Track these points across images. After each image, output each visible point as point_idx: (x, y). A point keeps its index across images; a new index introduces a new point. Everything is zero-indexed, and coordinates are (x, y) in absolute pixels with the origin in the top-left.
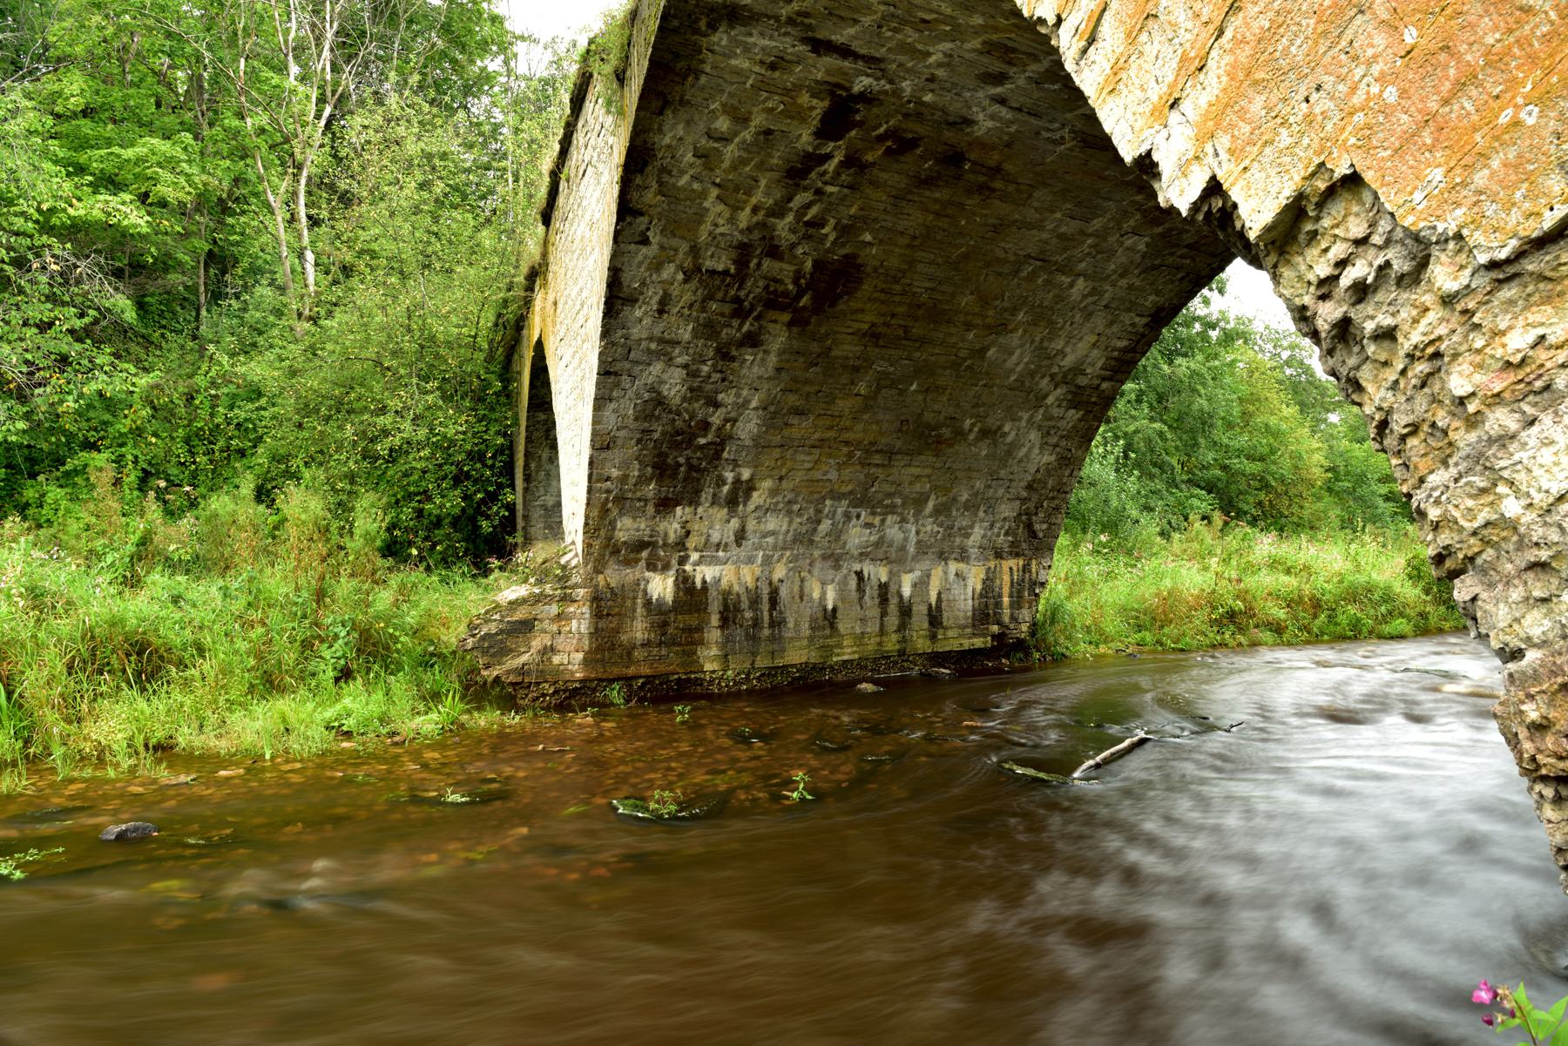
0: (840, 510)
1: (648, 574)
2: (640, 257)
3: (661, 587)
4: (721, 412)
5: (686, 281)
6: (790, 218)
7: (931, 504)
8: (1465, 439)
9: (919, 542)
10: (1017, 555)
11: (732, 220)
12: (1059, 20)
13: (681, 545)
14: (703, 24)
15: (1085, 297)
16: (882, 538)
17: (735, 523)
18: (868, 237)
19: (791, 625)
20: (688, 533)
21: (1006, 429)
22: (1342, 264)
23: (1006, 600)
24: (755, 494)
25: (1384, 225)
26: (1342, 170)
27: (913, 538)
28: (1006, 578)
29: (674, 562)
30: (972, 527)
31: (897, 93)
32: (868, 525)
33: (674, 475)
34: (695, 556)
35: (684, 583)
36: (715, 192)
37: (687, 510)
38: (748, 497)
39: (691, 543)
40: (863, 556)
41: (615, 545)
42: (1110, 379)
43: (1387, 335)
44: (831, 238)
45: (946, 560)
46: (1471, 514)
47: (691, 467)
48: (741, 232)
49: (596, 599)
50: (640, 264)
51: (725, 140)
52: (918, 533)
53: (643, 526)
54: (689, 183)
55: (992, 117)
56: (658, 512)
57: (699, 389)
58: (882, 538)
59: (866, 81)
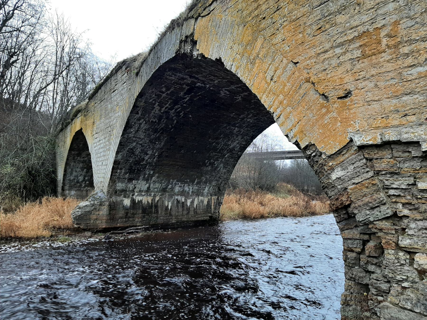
0: (174, 182)
1: (124, 199)
2: (136, 117)
3: (127, 202)
4: (148, 156)
5: (146, 123)
6: (174, 110)
7: (196, 182)
8: (326, 173)
9: (192, 191)
10: (216, 195)
11: (160, 110)
12: (273, 113)
13: (133, 191)
14: (167, 70)
15: (237, 132)
16: (183, 190)
17: (147, 185)
18: (190, 116)
19: (160, 213)
20: (135, 187)
21: (215, 163)
22: (312, 153)
23: (213, 207)
24: (153, 178)
25: (317, 150)
26: (313, 143)
27: (191, 190)
28: (213, 201)
29: (131, 196)
30: (205, 188)
31: (205, 87)
32: (180, 187)
33: (133, 172)
34: (136, 194)
35: (133, 201)
36: (157, 104)
37: (136, 181)
38: (151, 178)
39: (135, 190)
40: (178, 195)
41: (116, 190)
42: (240, 151)
43: (317, 162)
44: (182, 116)
45: (198, 196)
46: (326, 181)
47: (138, 170)
48: (162, 113)
49: (110, 205)
50: (135, 119)
51: (163, 93)
52: (192, 189)
53: (124, 185)
54: (152, 101)
55: (225, 93)
56: (128, 182)
57: (144, 150)
58: (183, 190)
59: (199, 84)
